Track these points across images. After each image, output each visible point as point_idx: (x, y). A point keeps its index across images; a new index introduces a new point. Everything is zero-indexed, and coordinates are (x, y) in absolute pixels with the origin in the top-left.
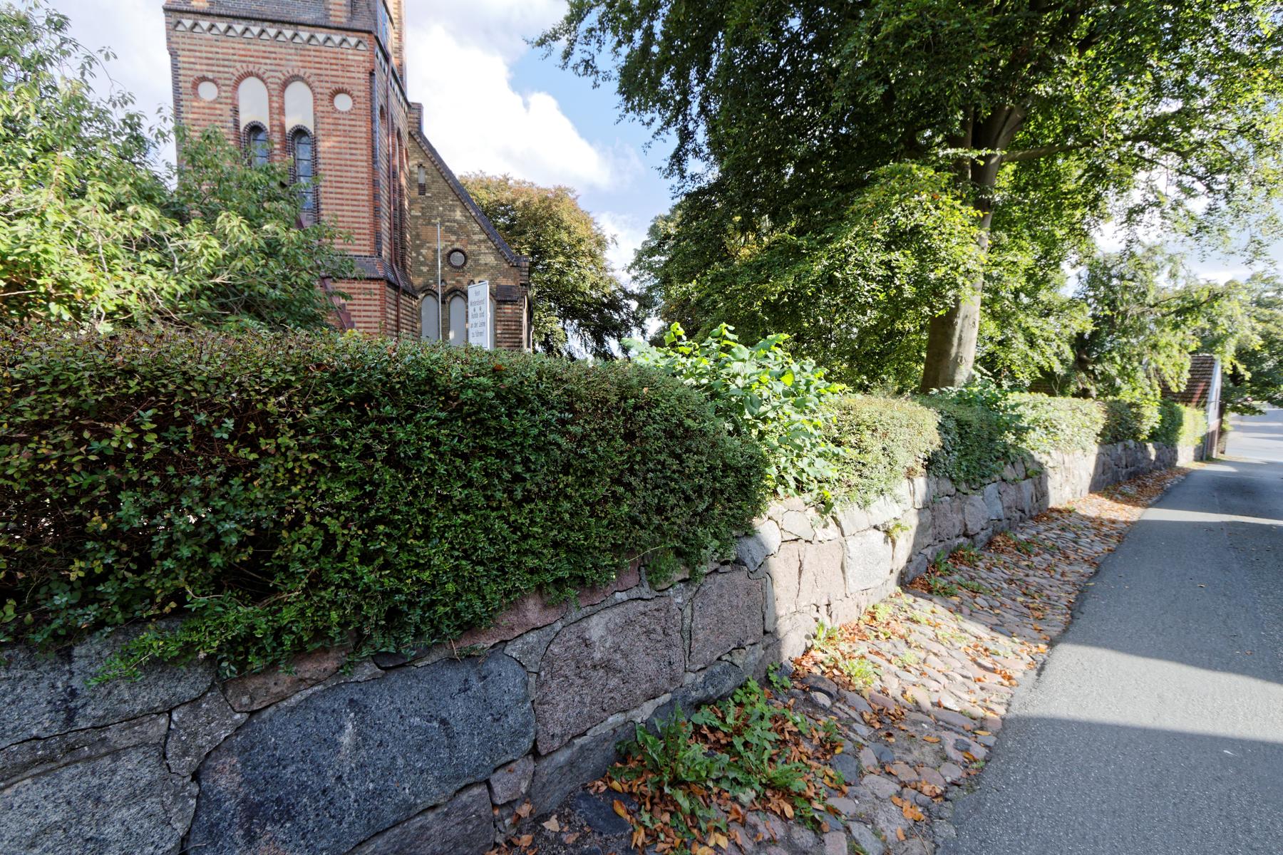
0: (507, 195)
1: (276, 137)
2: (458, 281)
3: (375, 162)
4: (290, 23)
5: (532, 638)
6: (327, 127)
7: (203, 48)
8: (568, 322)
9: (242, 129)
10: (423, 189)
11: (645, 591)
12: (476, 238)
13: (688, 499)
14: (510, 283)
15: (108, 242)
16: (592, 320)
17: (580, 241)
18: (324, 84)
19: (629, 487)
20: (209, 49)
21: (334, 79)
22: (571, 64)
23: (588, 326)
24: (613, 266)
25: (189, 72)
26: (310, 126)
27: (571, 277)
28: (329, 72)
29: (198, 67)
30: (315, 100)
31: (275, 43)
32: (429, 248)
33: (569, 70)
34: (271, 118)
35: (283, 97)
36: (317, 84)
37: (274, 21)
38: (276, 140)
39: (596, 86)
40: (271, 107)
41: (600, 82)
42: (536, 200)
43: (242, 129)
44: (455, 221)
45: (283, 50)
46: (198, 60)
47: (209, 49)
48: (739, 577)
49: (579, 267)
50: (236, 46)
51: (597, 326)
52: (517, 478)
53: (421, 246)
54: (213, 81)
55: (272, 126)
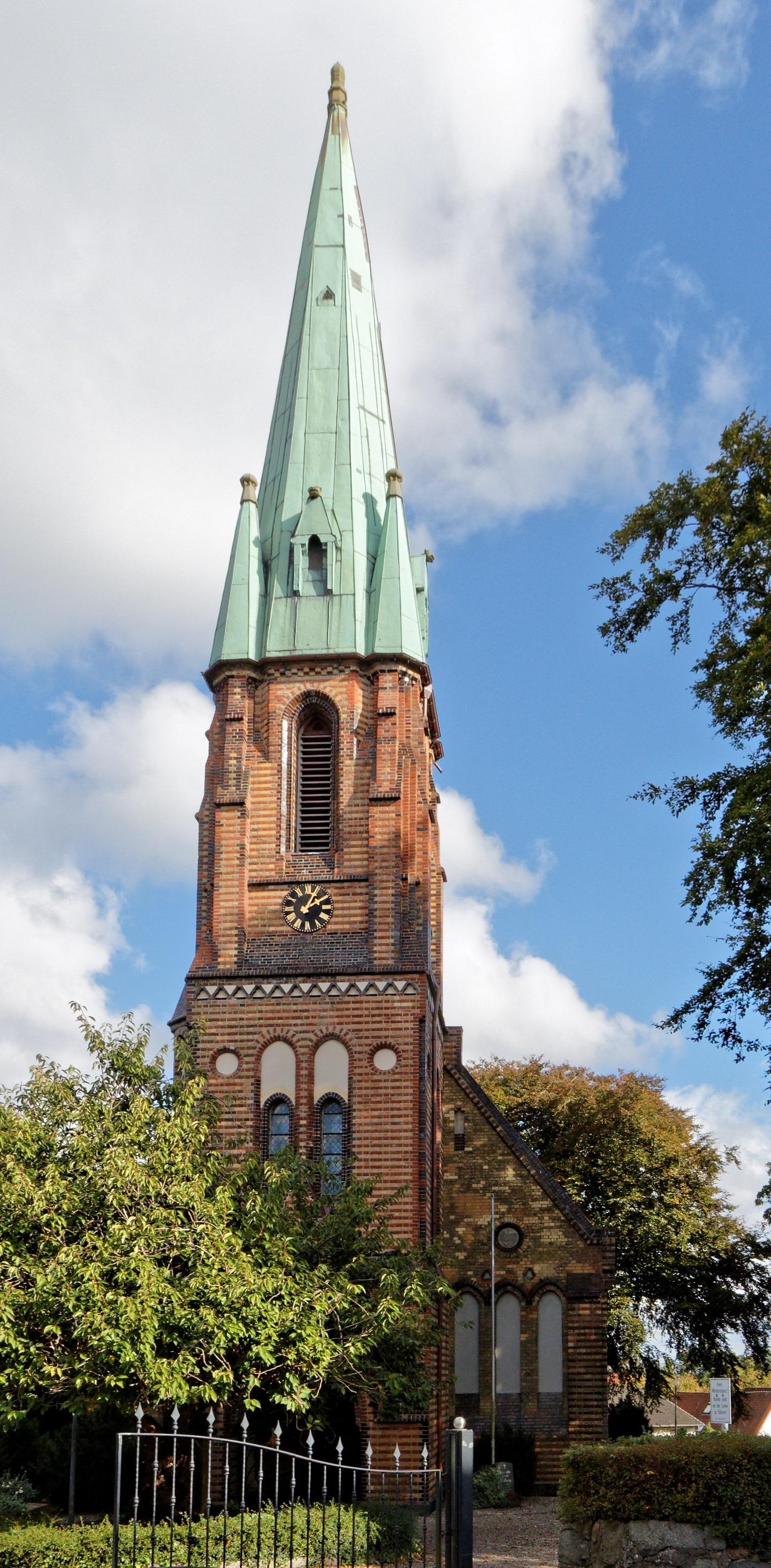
0: (542, 1095)
1: (303, 1111)
2: (509, 1272)
4: (327, 975)
6: (364, 1092)
7: (227, 1016)
8: (644, 1302)
10: (460, 1141)
12: (536, 1205)
14: (587, 1269)
15: (146, 1282)
16: (692, 1298)
17: (670, 1161)
18: (364, 1041)
20: (233, 1016)
21: (376, 1033)
22: (706, 1033)
23: (685, 1311)
24: (731, 1201)
25: (208, 1046)
26: (344, 1094)
27: (655, 1221)
28: (371, 1026)
29: (219, 1038)
30: (352, 1060)
32: (468, 1225)
34: (298, 1089)
35: (313, 1061)
36: (355, 1041)
37: (308, 976)
38: (303, 1115)
39: (740, 1058)
40: (298, 1076)
41: (744, 1053)
42: (592, 1100)
44: (505, 1184)
45: (317, 1007)
46: (220, 1031)
47: (233, 1016)
50: (264, 1008)
51: (703, 1308)
53: (457, 1223)
55: (298, 1098)
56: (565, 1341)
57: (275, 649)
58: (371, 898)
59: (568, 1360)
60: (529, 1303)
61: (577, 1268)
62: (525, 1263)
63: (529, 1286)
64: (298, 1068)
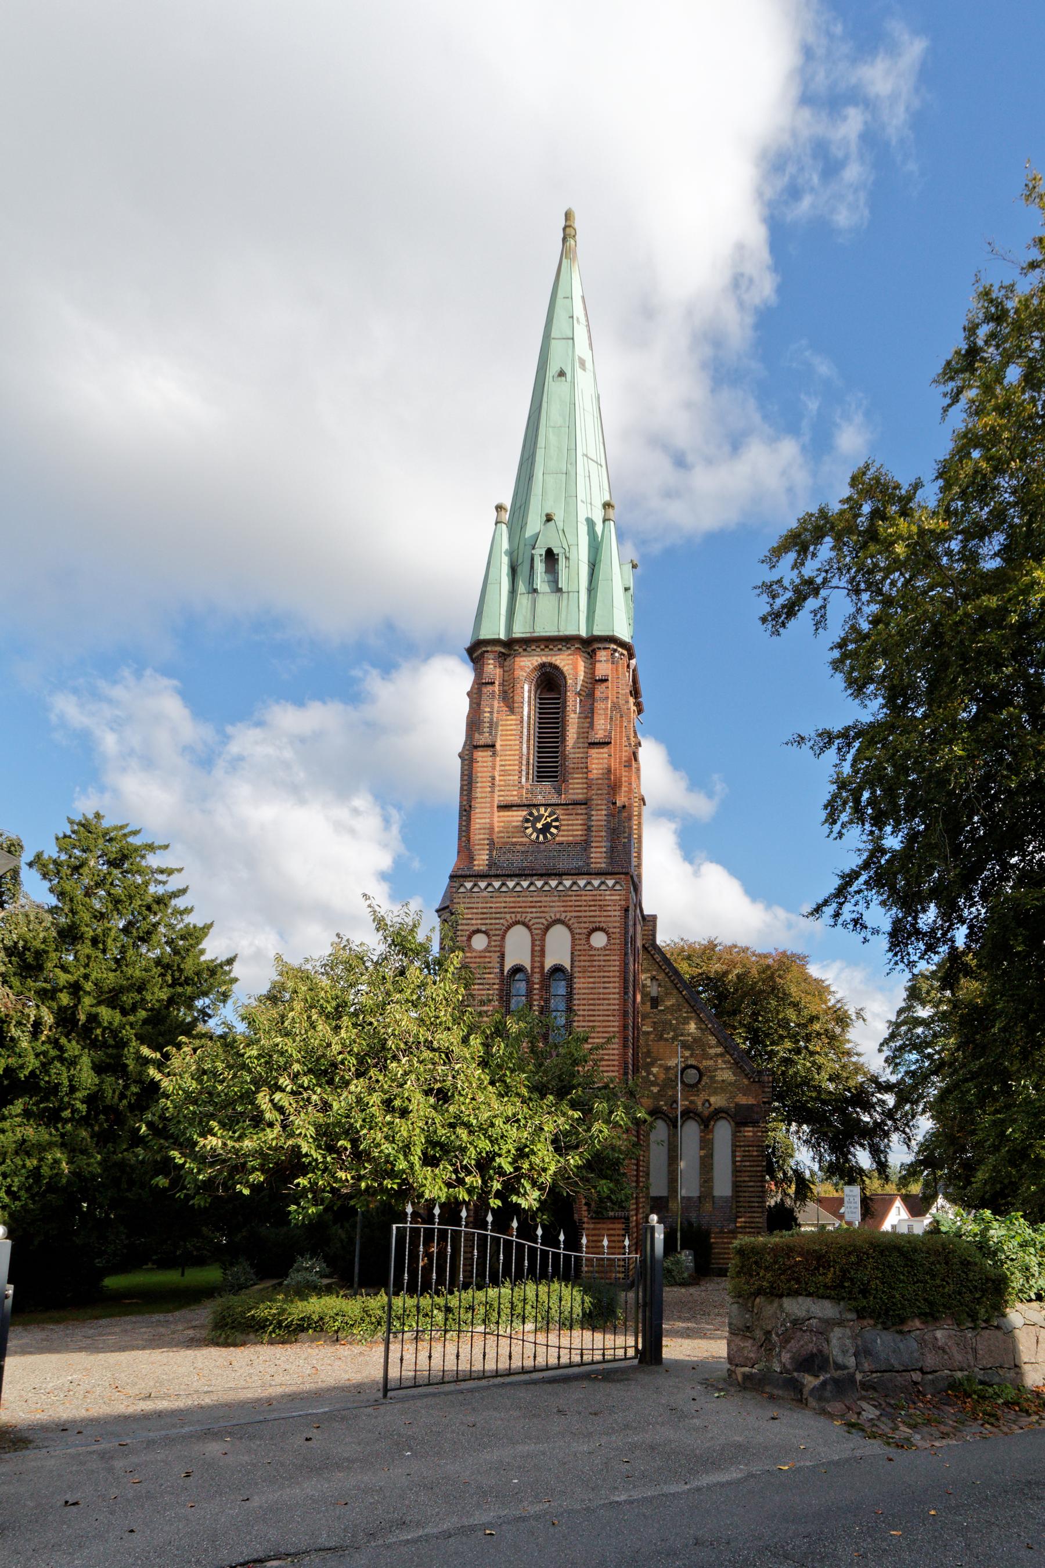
1: (536, 978)
2: (691, 1102)
3: (626, 993)
4: (555, 875)
5: (918, 1332)
6: (583, 964)
7: (480, 905)
8: (794, 1127)
9: (506, 972)
11: (955, 1327)
12: (712, 1051)
13: (971, 1292)
14: (751, 1101)
17: (813, 1019)
18: (583, 925)
19: (948, 1283)
21: (592, 919)
23: (825, 1134)
24: (859, 1049)
25: (466, 927)
27: (802, 1064)
28: (588, 914)
29: (474, 922)
30: (573, 939)
31: (541, 893)
32: (661, 1066)
33: (839, 926)
34: (533, 961)
36: (576, 925)
37: (542, 875)
39: (866, 940)
40: (533, 951)
41: (869, 936)
42: (754, 972)
43: (506, 972)
44: (689, 1035)
45: (548, 899)
46: (475, 916)
48: (999, 1334)
49: (812, 1053)
50: (508, 899)
52: (915, 1275)
53: (652, 1064)
54: (485, 932)
55: (533, 968)
56: (734, 1156)
57: (519, 632)
58: (589, 817)
59: (736, 1171)
60: (707, 1126)
61: (743, 1100)
62: (703, 1096)
63: (706, 1113)
64: (533, 945)
